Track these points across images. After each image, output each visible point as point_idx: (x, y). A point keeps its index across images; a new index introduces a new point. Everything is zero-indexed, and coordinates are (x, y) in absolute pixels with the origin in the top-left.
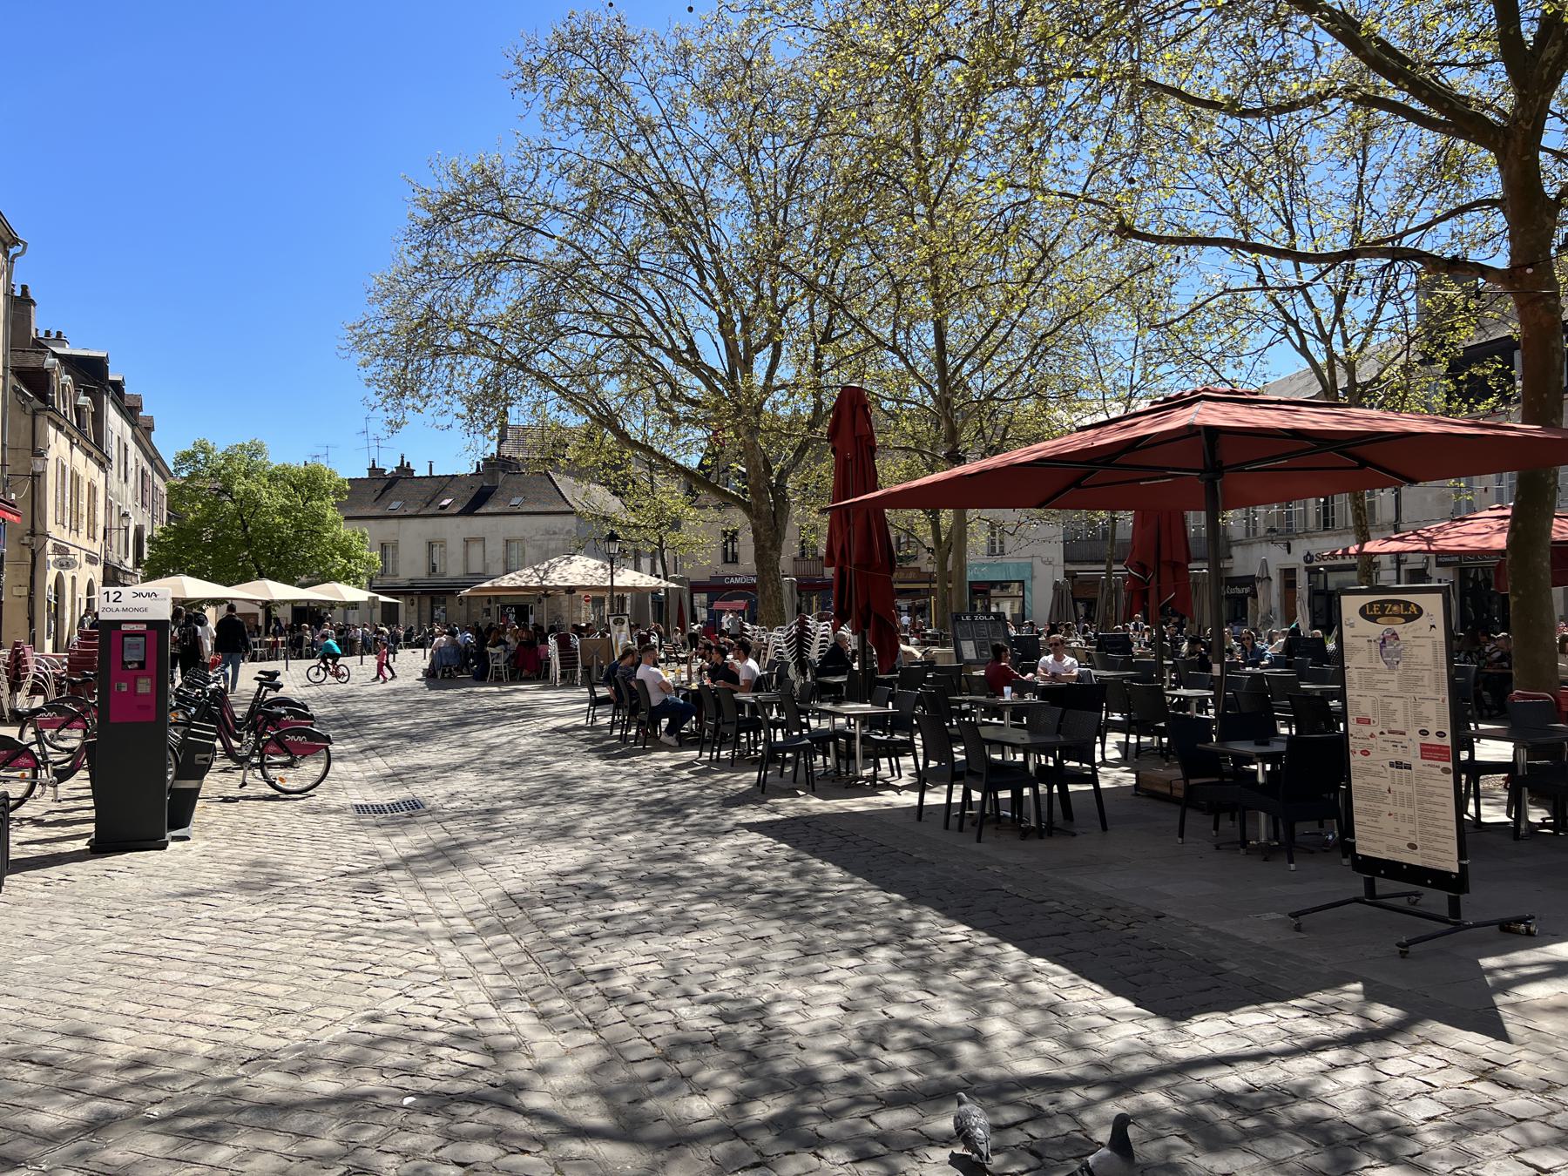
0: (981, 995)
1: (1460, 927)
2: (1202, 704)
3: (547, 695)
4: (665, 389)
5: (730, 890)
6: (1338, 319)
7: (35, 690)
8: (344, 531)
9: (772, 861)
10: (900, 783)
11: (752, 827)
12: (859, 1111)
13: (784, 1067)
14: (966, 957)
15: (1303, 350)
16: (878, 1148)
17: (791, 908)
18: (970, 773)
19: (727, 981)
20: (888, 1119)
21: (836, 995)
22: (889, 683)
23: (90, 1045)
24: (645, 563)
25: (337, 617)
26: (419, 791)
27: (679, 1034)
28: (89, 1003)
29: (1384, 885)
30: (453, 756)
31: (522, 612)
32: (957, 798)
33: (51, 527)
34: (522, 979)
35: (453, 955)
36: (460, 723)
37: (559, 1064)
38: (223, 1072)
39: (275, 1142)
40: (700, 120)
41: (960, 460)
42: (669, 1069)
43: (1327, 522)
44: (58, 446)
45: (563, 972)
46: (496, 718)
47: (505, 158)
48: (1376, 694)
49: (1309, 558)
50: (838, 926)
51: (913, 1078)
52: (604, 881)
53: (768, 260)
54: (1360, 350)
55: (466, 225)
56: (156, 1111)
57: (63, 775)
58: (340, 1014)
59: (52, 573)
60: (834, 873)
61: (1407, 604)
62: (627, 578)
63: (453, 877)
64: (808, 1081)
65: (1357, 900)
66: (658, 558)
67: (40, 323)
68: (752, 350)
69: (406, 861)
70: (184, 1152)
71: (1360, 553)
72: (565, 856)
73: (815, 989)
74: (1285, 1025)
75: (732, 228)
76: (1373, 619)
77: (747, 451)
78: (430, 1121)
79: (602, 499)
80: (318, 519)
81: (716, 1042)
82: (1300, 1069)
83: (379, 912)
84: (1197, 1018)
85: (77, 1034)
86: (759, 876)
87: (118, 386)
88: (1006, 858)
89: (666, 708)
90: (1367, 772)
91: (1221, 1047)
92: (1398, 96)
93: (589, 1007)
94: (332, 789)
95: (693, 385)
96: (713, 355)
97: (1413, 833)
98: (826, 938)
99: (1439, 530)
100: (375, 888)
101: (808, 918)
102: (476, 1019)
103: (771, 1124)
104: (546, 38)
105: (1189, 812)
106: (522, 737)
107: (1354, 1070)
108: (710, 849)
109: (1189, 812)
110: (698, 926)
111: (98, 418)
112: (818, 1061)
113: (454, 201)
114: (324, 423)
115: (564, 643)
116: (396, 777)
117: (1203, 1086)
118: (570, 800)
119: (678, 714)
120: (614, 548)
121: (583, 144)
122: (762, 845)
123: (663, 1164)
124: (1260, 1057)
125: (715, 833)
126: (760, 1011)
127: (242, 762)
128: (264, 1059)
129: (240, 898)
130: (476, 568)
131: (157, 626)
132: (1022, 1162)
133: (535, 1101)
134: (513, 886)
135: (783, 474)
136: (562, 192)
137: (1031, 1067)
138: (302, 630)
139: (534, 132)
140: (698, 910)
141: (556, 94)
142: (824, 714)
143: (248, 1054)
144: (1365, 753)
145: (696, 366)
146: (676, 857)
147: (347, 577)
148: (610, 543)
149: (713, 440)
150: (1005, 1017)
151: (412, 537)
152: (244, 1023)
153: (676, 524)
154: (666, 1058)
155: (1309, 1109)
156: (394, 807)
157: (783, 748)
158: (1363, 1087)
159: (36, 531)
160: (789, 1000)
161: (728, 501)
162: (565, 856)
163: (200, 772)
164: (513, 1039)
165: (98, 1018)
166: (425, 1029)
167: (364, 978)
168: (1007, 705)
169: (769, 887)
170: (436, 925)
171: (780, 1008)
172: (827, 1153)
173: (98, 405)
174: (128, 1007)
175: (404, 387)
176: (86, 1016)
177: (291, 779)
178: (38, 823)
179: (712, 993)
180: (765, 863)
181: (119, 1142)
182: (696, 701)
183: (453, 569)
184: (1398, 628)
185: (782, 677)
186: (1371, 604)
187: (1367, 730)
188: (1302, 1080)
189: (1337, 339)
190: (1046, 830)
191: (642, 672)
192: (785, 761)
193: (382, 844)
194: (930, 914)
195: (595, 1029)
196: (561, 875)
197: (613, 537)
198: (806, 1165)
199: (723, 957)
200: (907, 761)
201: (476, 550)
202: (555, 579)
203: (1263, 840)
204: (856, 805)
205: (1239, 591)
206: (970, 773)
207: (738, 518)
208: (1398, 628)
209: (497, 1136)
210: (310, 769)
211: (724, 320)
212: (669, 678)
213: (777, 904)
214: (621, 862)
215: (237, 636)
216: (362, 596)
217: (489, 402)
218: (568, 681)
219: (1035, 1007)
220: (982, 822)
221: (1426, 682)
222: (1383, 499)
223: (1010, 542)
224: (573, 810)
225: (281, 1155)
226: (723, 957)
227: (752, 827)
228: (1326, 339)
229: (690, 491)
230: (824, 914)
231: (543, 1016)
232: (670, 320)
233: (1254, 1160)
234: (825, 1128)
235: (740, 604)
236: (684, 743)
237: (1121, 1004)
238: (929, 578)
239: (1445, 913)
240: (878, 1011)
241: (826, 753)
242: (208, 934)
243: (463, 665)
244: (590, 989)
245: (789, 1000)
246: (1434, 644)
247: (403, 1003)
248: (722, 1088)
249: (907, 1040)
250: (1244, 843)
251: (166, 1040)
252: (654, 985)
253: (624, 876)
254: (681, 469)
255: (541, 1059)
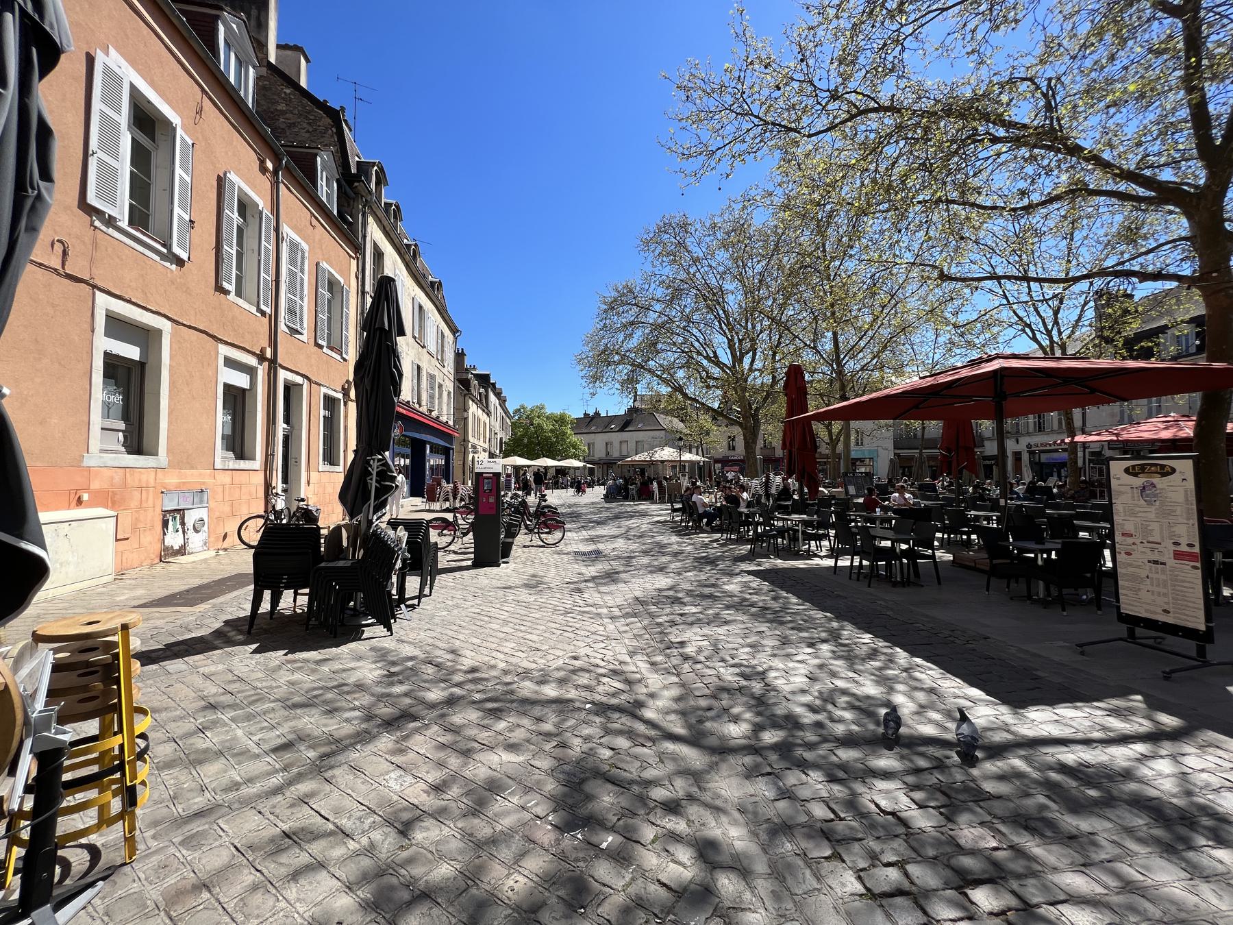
0: (888, 679)
1: (1206, 664)
2: (988, 519)
3: (653, 506)
4: (704, 374)
5: (741, 605)
6: (1056, 322)
7: (462, 500)
8: (574, 438)
9: (762, 593)
10: (822, 554)
11: (749, 573)
12: (827, 746)
13: (780, 711)
14: (873, 654)
15: (1034, 339)
16: (841, 775)
17: (775, 618)
18: (864, 552)
19: (743, 654)
20: (846, 754)
21: (803, 669)
22: (813, 505)
23: (456, 658)
24: (694, 450)
25: (572, 471)
26: (601, 546)
27: (721, 683)
28: (460, 637)
29: (1139, 631)
30: (614, 531)
31: (643, 471)
32: (856, 563)
33: (471, 439)
34: (642, 643)
35: (611, 627)
36: (617, 517)
37: (661, 696)
38: (508, 679)
39: (526, 722)
40: (722, 255)
41: (848, 399)
42: (715, 703)
43: (1040, 428)
44: (473, 408)
45: (661, 641)
46: (631, 516)
47: (637, 281)
48: (1138, 520)
49: (1029, 446)
50: (799, 629)
51: (854, 728)
52: (680, 595)
53: (750, 312)
54: (1069, 337)
55: (621, 309)
56: (478, 696)
57: (465, 534)
58: (560, 653)
59: (471, 456)
60: (794, 600)
61: (1163, 467)
62: (687, 456)
63: (613, 588)
64: (792, 722)
65: (1121, 639)
66: (700, 448)
67: (468, 362)
68: (742, 355)
69: (594, 578)
70: (486, 722)
71: (1072, 442)
72: (662, 581)
73: (791, 665)
74: (1097, 720)
75: (734, 301)
76: (1135, 475)
77: (742, 401)
78: (598, 720)
79: (677, 424)
80: (565, 434)
81: (740, 689)
82: (1121, 755)
83: (581, 603)
84: (1031, 708)
85: (453, 652)
86: (755, 598)
87: (494, 385)
88: (888, 598)
89: (705, 514)
90: (1130, 565)
91: (1056, 731)
92: (1111, 186)
93: (675, 661)
94: (566, 544)
95: (715, 371)
96: (725, 357)
97: (1167, 603)
98: (794, 635)
99: (1123, 429)
100: (580, 591)
101: (782, 623)
102: (621, 663)
103: (775, 747)
104: (653, 228)
105: (992, 579)
106: (644, 524)
107: (1160, 761)
108: (729, 583)
109: (992, 579)
110: (726, 623)
111: (487, 397)
112: (798, 710)
113: (615, 300)
114: (566, 394)
115: (660, 484)
116: (592, 540)
117: (1049, 759)
118: (663, 554)
119: (711, 517)
120: (681, 443)
121: (668, 271)
122: (755, 582)
123: (717, 764)
124: (1087, 742)
125: (731, 574)
126: (762, 675)
127: (531, 531)
128: (525, 674)
129: (525, 591)
130: (624, 453)
131: (497, 475)
132: (937, 800)
133: (649, 714)
134: (639, 594)
135: (757, 410)
136: (660, 292)
137: (928, 730)
138: (559, 478)
139: (649, 269)
140: (727, 614)
141: (657, 252)
142: (779, 519)
143: (520, 670)
144: (1128, 554)
145: (718, 363)
146: (713, 585)
147: (576, 457)
148: (678, 441)
149: (724, 395)
150: (904, 694)
151: (600, 440)
152: (519, 654)
153: (708, 433)
154: (714, 696)
155: (1133, 786)
156: (590, 553)
157: (762, 535)
158: (1174, 775)
159: (466, 440)
160: (777, 670)
161: (732, 422)
162: (662, 581)
163: (514, 536)
164: (638, 676)
165: (462, 644)
166: (598, 666)
167: (572, 636)
168: (877, 518)
169: (761, 604)
170: (605, 611)
171: (772, 674)
172: (811, 773)
173: (487, 392)
174: (475, 641)
175: (596, 378)
176: (457, 643)
177: (550, 539)
178: (455, 553)
179: (736, 661)
180: (757, 592)
181: (460, 712)
182: (719, 511)
183: (616, 454)
184: (1155, 481)
185: (759, 501)
186: (1134, 467)
187: (1130, 540)
188: (1126, 764)
189: (1055, 333)
190: (905, 583)
191: (694, 498)
192: (763, 541)
193: (584, 570)
194: (849, 626)
195: (678, 675)
196: (660, 590)
197: (680, 439)
198: (799, 780)
199: (740, 641)
200: (825, 543)
201: (624, 446)
202: (657, 457)
203: (1041, 596)
204: (801, 564)
205: (988, 462)
206: (864, 552)
207: (737, 431)
208: (1155, 481)
209: (630, 734)
210: (558, 535)
211: (730, 341)
212: (707, 501)
213: (763, 613)
214: (686, 586)
215: (541, 477)
216: (580, 464)
217: (629, 383)
218: (662, 501)
219: (922, 689)
220: (871, 576)
221: (1178, 513)
222: (1077, 413)
223: (866, 440)
224: (665, 559)
225: (528, 730)
226: (740, 641)
227: (749, 573)
228: (1049, 333)
229: (714, 418)
230: (791, 622)
231: (653, 664)
232: (707, 344)
233: (1109, 825)
234: (808, 755)
235: (737, 468)
236: (714, 531)
237: (975, 692)
238: (827, 457)
239: (1194, 654)
240: (828, 684)
241: (783, 538)
242: (510, 607)
243: (619, 493)
244: (675, 652)
245: (777, 670)
246: (1186, 490)
247: (588, 651)
248: (746, 720)
249: (847, 702)
250: (1029, 597)
251: (487, 659)
252: (706, 653)
253: (689, 593)
254: (710, 409)
255: (652, 689)
